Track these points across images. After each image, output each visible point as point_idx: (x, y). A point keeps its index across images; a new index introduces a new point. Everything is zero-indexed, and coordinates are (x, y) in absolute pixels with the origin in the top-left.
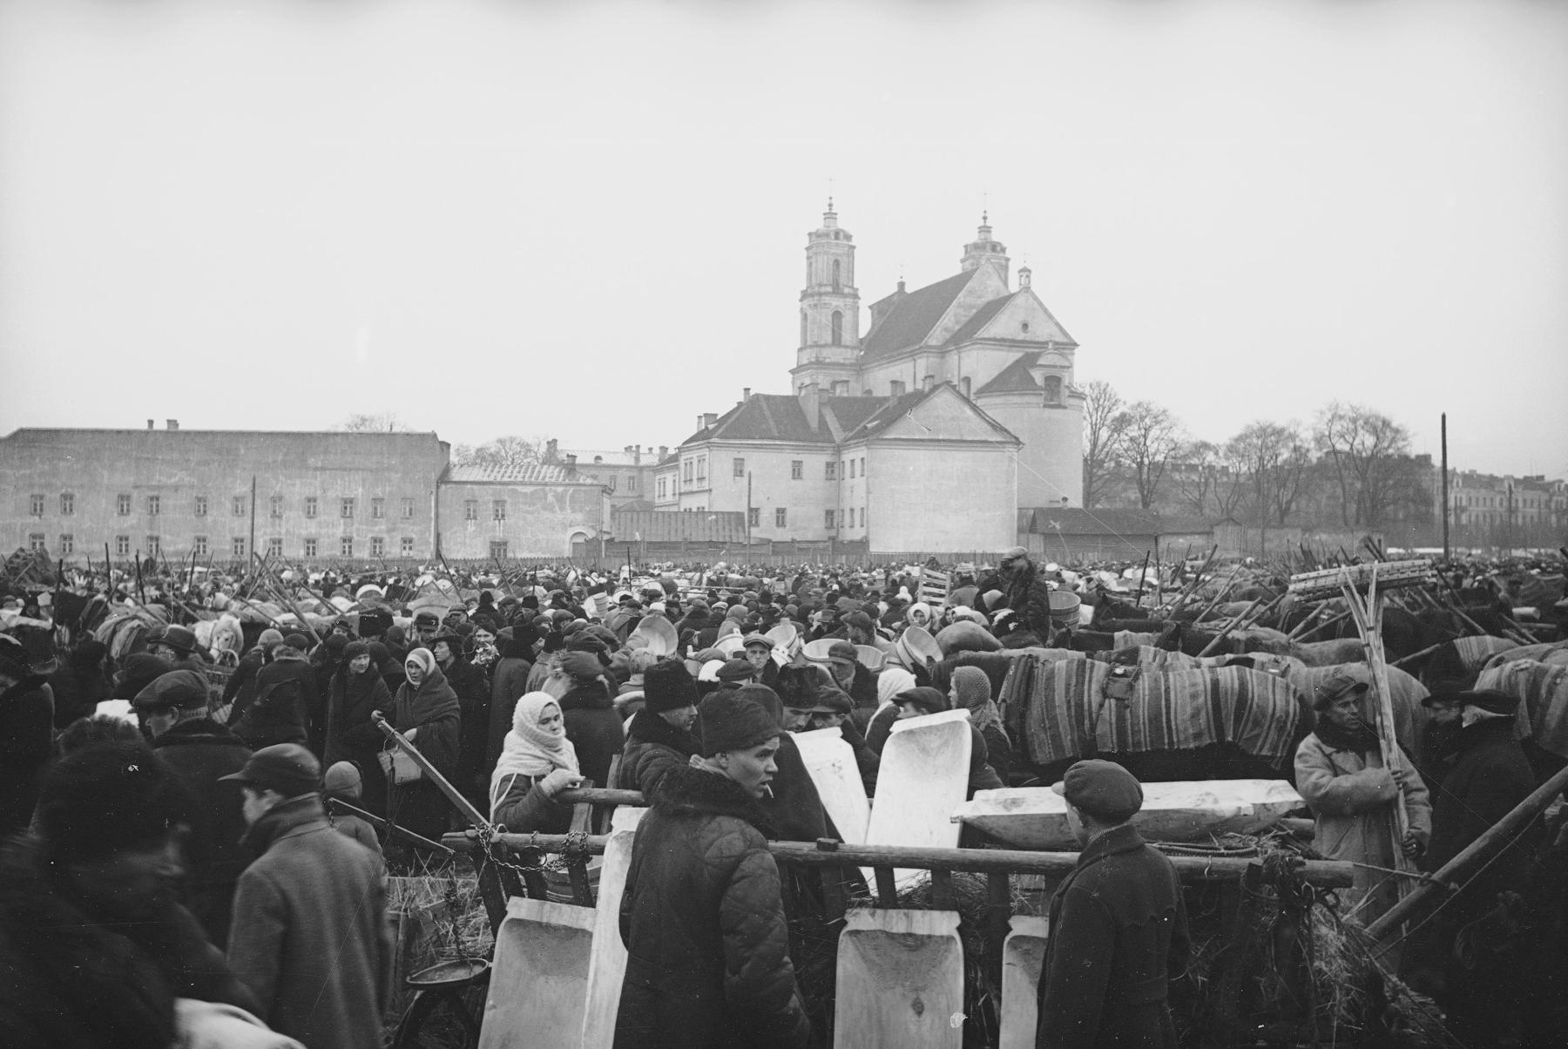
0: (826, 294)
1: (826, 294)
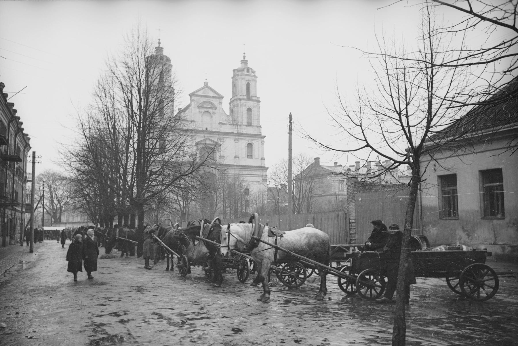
0: (243, 99)
1: (243, 99)
